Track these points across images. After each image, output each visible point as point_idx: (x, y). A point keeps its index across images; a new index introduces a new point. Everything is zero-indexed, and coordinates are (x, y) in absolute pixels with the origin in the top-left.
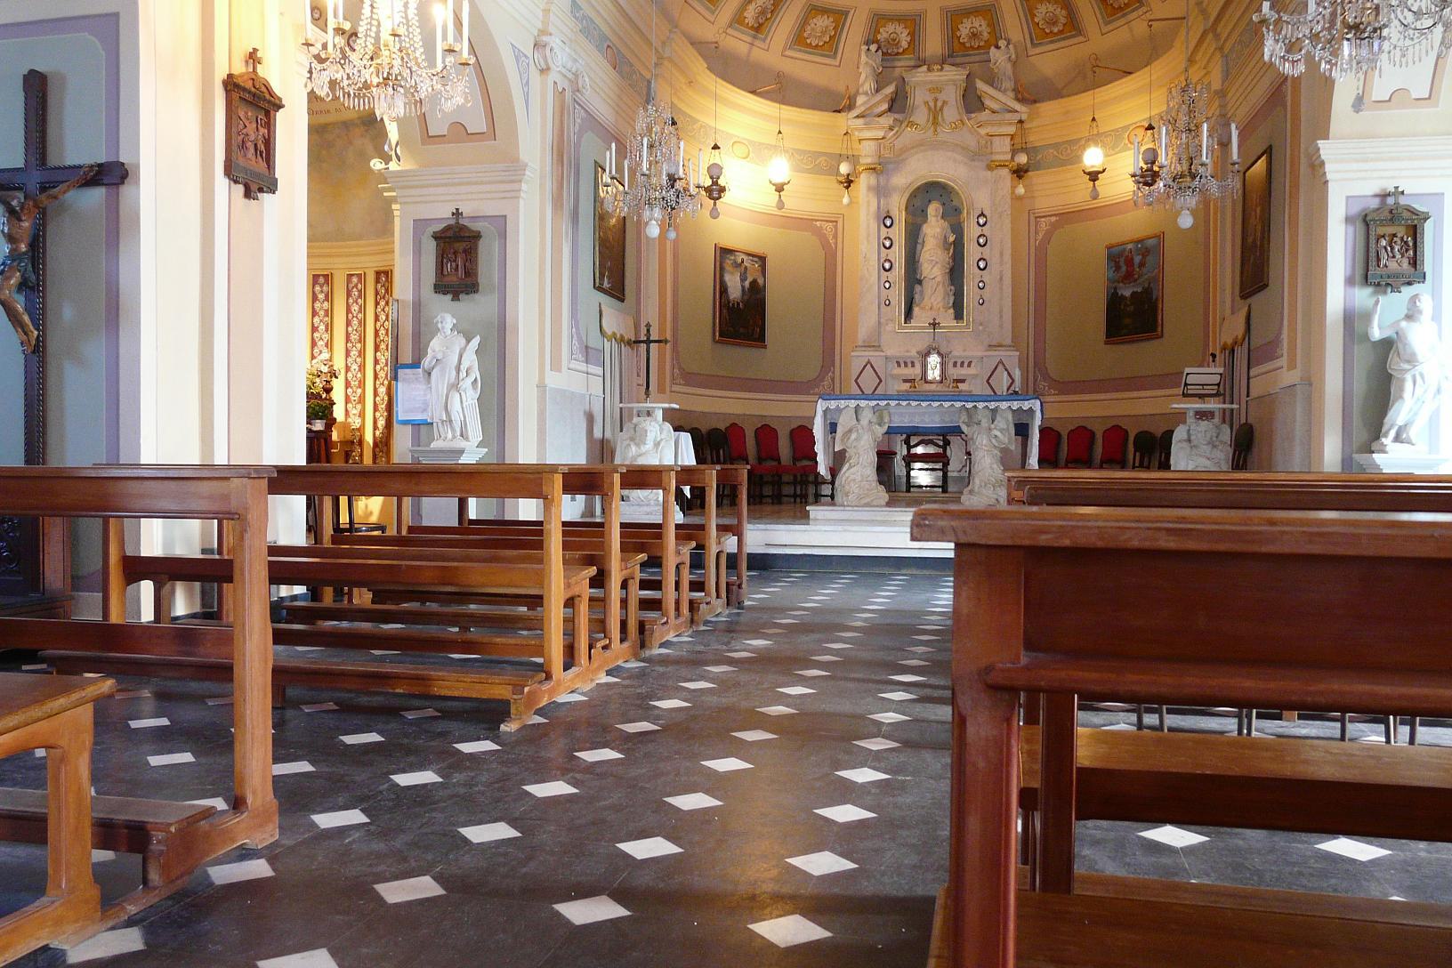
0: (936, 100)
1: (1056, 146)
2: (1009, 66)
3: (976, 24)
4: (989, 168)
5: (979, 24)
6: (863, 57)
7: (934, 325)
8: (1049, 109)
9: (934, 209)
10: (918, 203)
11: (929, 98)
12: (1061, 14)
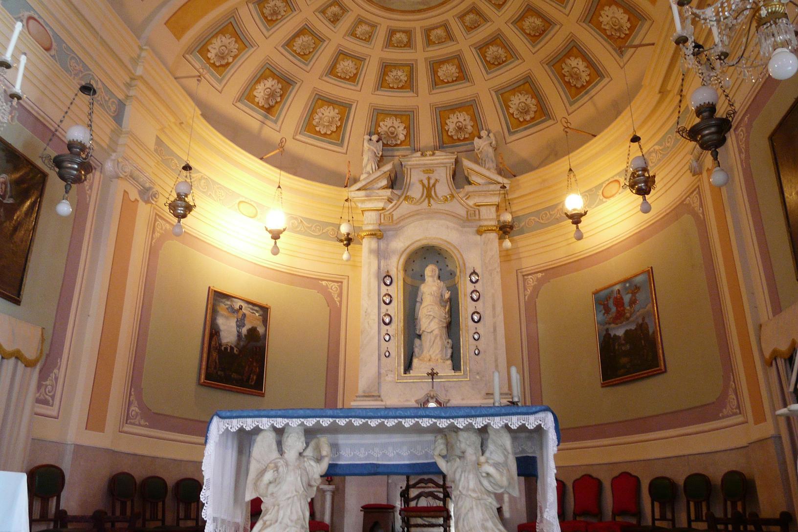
0: (429, 179)
1: (537, 213)
2: (491, 150)
3: (461, 119)
4: (479, 232)
5: (462, 118)
6: (366, 144)
7: (433, 375)
8: (528, 181)
9: (430, 271)
10: (416, 267)
11: (424, 177)
12: (531, 102)
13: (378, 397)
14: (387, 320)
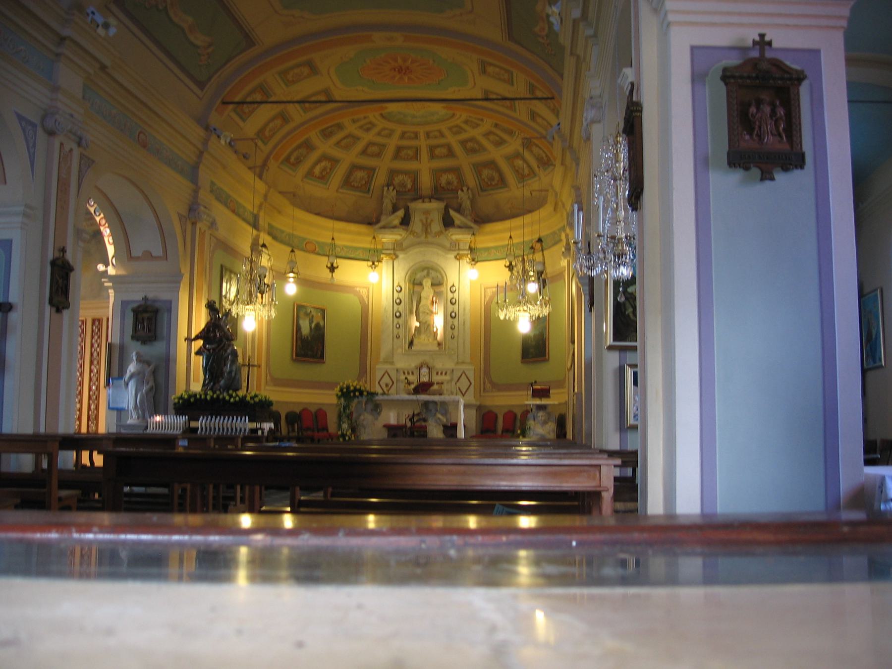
0: (427, 219)
2: (468, 203)
5: (451, 177)
13: (392, 363)
14: (398, 314)
